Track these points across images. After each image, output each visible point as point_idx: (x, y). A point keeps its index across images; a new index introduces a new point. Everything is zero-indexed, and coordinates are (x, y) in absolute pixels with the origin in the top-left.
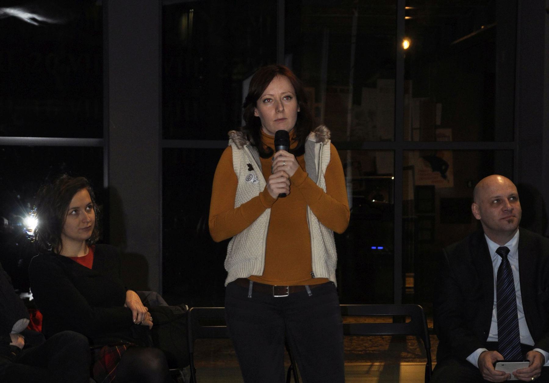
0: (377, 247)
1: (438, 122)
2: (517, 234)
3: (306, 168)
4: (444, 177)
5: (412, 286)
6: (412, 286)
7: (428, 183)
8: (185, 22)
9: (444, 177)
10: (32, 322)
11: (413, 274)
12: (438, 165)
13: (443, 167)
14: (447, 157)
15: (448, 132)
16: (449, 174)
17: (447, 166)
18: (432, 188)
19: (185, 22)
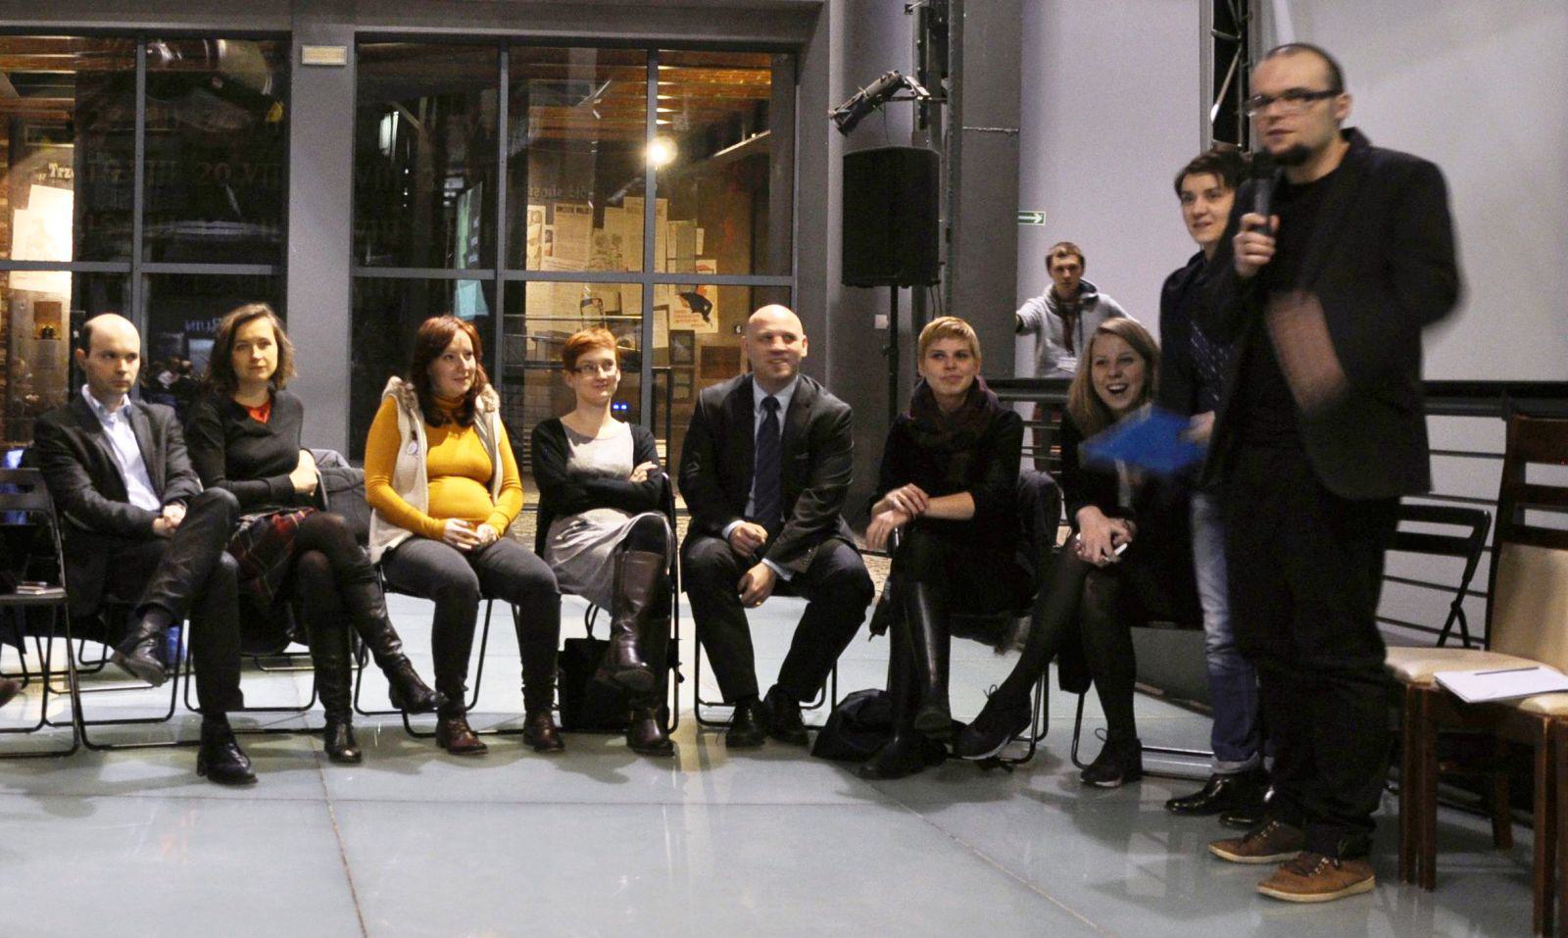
0: (620, 406)
1: (700, 252)
2: (370, 653)
3: (1067, 817)
4: (706, 319)
5: (1396, 561)
6: (1396, 561)
7: (686, 327)
8: (388, 128)
9: (706, 319)
10: (236, 484)
11: (664, 441)
12: (698, 304)
13: (706, 308)
14: (711, 293)
15: (712, 264)
16: (713, 315)
17: (710, 306)
18: (691, 334)
19: (388, 128)
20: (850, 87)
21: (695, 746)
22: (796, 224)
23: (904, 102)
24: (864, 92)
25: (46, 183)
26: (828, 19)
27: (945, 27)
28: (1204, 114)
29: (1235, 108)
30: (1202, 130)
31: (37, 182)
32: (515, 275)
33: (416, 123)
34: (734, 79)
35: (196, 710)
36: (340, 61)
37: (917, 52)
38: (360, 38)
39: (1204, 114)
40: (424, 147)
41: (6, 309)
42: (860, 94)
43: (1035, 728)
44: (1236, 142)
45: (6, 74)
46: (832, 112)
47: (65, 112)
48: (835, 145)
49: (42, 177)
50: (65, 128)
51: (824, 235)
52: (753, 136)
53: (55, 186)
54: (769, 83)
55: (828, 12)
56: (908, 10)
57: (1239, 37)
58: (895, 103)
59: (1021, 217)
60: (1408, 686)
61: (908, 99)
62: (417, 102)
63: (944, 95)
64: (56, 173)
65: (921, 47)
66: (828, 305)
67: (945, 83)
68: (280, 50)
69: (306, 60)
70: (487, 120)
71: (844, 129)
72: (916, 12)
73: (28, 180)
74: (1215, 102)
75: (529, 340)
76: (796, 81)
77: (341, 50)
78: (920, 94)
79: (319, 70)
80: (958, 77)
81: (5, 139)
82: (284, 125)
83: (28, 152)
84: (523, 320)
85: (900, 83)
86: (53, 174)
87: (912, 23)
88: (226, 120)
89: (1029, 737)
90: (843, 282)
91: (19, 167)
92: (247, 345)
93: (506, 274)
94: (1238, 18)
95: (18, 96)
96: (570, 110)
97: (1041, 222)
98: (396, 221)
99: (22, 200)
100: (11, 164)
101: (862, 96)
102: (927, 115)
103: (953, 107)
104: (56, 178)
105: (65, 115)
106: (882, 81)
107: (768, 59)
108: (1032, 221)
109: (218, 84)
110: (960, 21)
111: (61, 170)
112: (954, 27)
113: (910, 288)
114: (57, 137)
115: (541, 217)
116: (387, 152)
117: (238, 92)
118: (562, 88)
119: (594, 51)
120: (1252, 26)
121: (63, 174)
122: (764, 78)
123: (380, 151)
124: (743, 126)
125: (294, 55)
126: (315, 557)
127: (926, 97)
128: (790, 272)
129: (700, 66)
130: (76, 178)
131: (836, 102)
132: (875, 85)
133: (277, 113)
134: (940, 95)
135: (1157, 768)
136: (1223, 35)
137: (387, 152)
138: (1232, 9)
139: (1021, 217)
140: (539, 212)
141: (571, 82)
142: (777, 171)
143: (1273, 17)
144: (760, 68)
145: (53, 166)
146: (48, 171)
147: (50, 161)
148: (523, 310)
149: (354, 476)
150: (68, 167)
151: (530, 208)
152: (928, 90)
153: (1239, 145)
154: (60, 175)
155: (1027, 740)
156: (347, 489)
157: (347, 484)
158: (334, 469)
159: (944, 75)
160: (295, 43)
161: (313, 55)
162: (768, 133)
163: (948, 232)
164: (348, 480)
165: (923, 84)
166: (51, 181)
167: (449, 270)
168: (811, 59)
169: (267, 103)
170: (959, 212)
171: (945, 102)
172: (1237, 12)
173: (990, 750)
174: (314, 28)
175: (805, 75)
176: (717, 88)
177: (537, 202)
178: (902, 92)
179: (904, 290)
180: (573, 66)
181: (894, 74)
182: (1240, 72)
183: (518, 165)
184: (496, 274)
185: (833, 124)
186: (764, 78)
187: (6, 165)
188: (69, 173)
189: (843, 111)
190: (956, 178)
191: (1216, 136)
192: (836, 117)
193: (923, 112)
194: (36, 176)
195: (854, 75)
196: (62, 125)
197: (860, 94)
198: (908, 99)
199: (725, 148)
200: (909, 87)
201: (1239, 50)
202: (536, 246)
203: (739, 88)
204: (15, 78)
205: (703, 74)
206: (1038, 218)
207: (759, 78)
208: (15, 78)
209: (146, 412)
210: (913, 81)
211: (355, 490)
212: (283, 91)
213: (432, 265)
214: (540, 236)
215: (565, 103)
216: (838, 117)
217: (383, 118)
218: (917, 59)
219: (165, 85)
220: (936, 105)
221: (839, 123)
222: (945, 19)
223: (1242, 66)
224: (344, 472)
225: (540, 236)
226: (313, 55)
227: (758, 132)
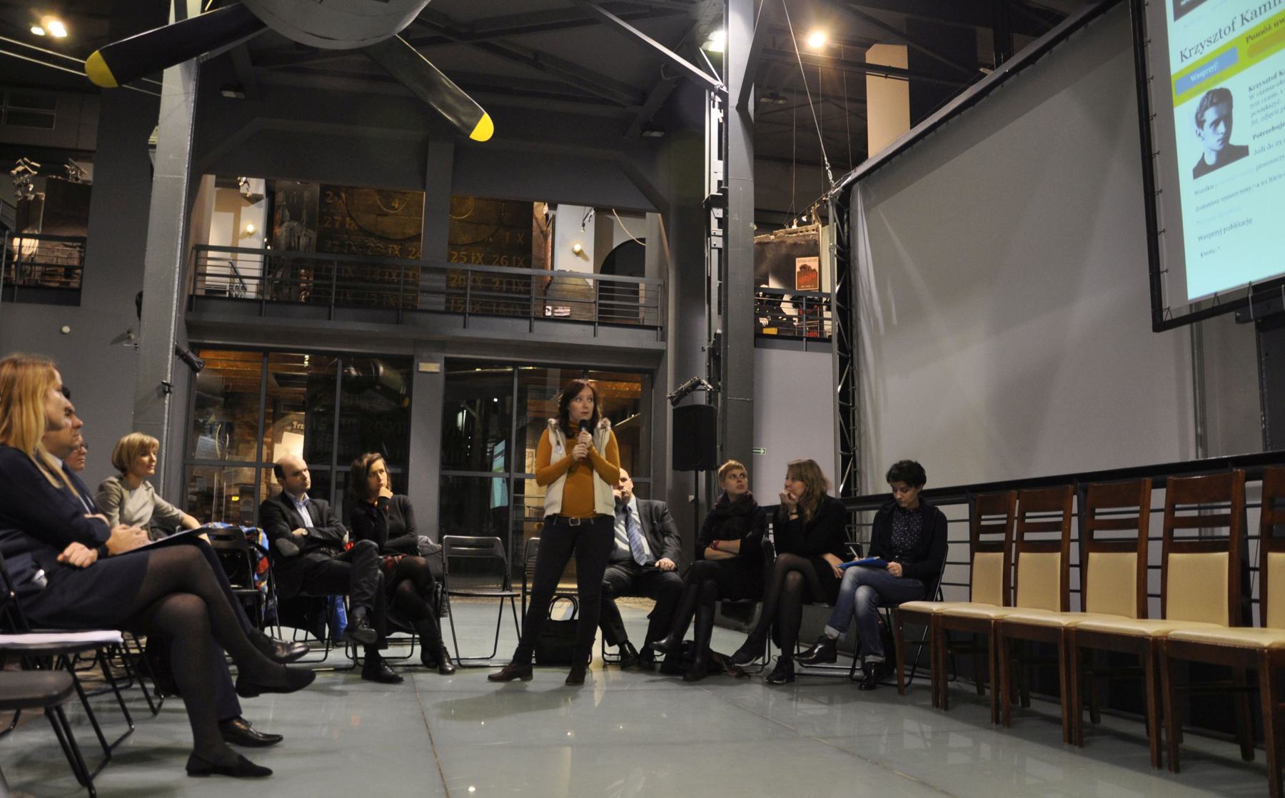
8: (461, 418)
19: (461, 418)
20: (677, 384)
25: (291, 431)
28: (835, 389)
32: (519, 476)
34: (624, 387)
38: (446, 359)
39: (835, 389)
40: (478, 426)
56: (703, 350)
65: (709, 367)
68: (405, 365)
71: (673, 404)
73: (283, 429)
80: (726, 379)
82: (410, 407)
83: (283, 415)
85: (699, 383)
87: (705, 356)
91: (278, 423)
92: (375, 474)
94: (849, 347)
96: (547, 402)
98: (461, 453)
105: (302, 398)
110: (726, 349)
114: (297, 409)
117: (389, 392)
118: (544, 391)
123: (457, 428)
126: (405, 585)
131: (670, 391)
132: (688, 383)
134: (717, 388)
135: (869, 476)
142: (643, 429)
148: (523, 492)
160: (416, 361)
161: (425, 367)
166: (296, 431)
174: (425, 354)
178: (700, 387)
186: (637, 387)
188: (302, 426)
190: (724, 420)
204: (277, 377)
205: (609, 384)
208: (277, 377)
209: (314, 504)
210: (704, 382)
213: (481, 470)
216: (671, 398)
220: (716, 393)
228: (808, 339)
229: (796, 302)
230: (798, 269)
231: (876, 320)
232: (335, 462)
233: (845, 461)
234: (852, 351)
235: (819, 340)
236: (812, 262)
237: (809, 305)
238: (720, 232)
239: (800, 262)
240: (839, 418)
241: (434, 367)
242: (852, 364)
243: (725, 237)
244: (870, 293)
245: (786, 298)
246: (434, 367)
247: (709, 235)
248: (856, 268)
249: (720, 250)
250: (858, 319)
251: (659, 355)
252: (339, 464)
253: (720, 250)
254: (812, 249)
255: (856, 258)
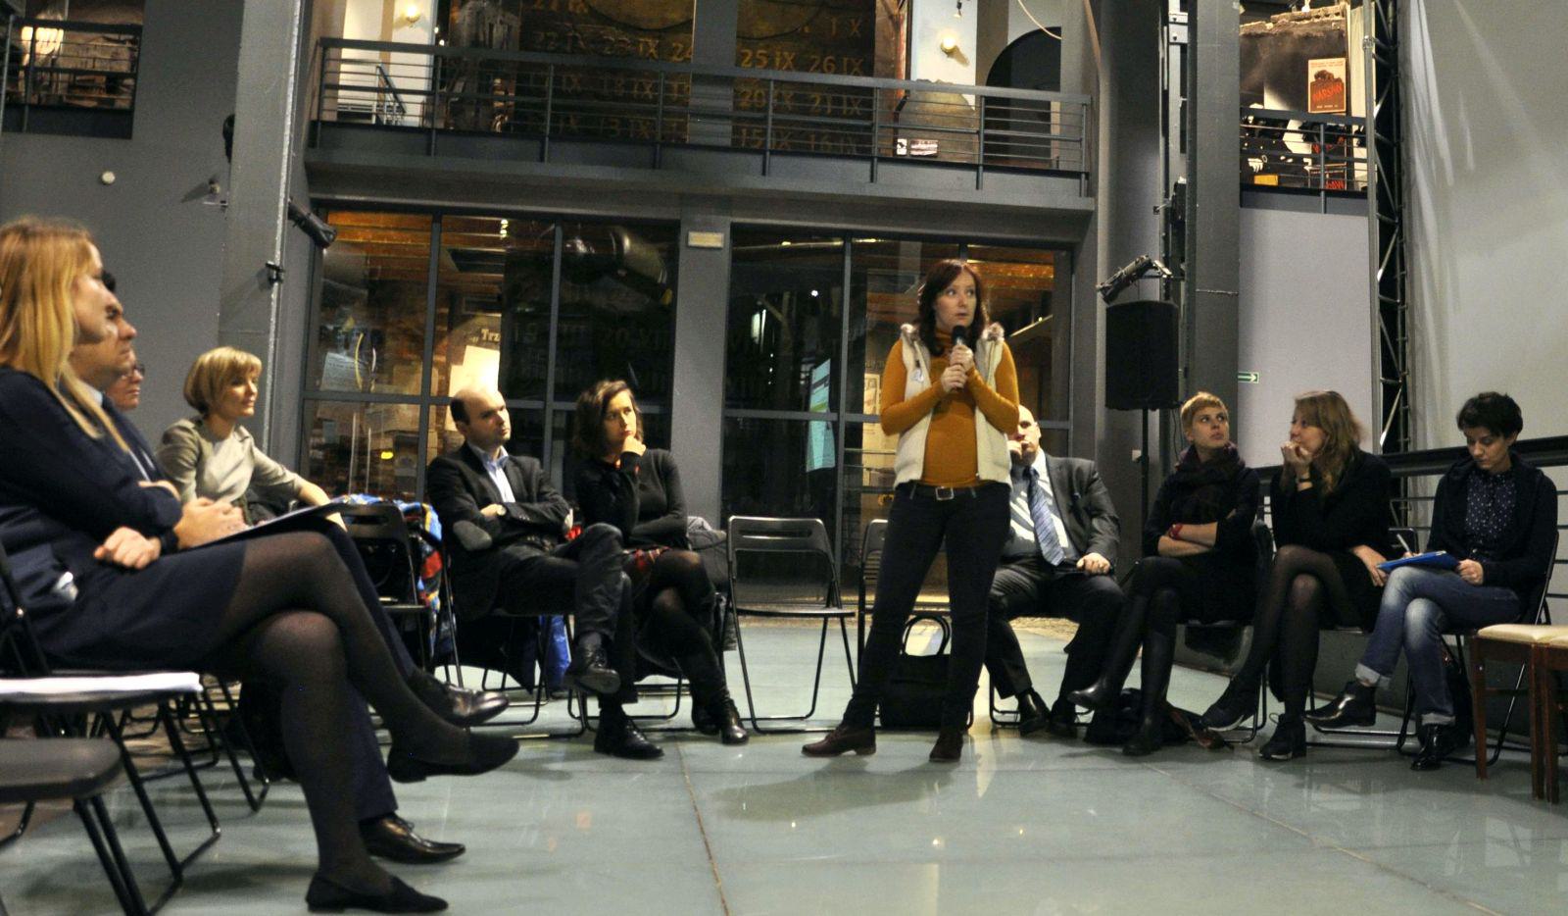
8: (758, 323)
19: (758, 323)
20: (1113, 266)
21: (991, 741)
22: (1072, 381)
23: (1153, 280)
24: (1122, 271)
25: (479, 344)
26: (1096, 224)
27: (1182, 222)
28: (1372, 275)
29: (1398, 437)
30: (1371, 286)
31: (471, 344)
32: (854, 418)
33: (779, 316)
34: (1026, 272)
35: (578, 718)
36: (719, 245)
37: (1162, 241)
39: (1372, 275)
40: (786, 337)
41: (441, 446)
42: (1119, 273)
43: (1256, 721)
44: (1398, 379)
45: (449, 251)
46: (1099, 286)
47: (496, 286)
48: (1101, 307)
49: (475, 339)
50: (495, 300)
51: (1093, 389)
52: (1040, 319)
53: (486, 347)
54: (1052, 276)
55: (1096, 218)
57: (1398, 301)
58: (1147, 280)
59: (1240, 377)
60: (1533, 646)
61: (1157, 277)
62: (781, 297)
63: (1182, 274)
64: (487, 337)
65: (1166, 239)
66: (1096, 444)
67: (1183, 267)
69: (692, 243)
70: (835, 312)
71: (1107, 299)
72: (1162, 212)
73: (465, 342)
74: (1380, 268)
75: (865, 470)
76: (1072, 272)
77: (720, 236)
78: (1164, 273)
79: (698, 251)
80: (1193, 260)
81: (446, 307)
83: (465, 319)
84: (860, 455)
85: (1149, 265)
86: (484, 338)
87: (1158, 221)
88: (627, 301)
89: (1251, 727)
90: (1106, 405)
93: (847, 417)
94: (1395, 206)
95: (457, 270)
96: (899, 296)
97: (1256, 380)
99: (459, 359)
100: (450, 329)
101: (1122, 274)
102: (1170, 286)
103: (1188, 283)
104: (487, 340)
105: (497, 290)
106: (1137, 263)
107: (1049, 255)
108: (1249, 380)
109: (622, 273)
110: (1194, 210)
111: (492, 335)
112: (1190, 215)
113: (1158, 411)
114: (488, 308)
115: (876, 382)
116: (757, 341)
118: (894, 279)
119: (919, 244)
120: (1405, 212)
121: (493, 337)
122: (1047, 272)
123: (752, 340)
124: (1033, 311)
125: (682, 237)
127: (1169, 276)
128: (1068, 418)
129: (1000, 261)
130: (502, 339)
131: (1102, 279)
132: (1131, 265)
133: (668, 299)
134: (1179, 274)
136: (1385, 218)
137: (757, 341)
138: (1392, 353)
139: (1240, 377)
140: (875, 379)
141: (901, 272)
143: (1419, 204)
144: (1046, 264)
145: (485, 331)
146: (481, 335)
147: (483, 327)
149: (716, 537)
150: (496, 332)
151: (867, 375)
152: (1171, 270)
153: (1398, 301)
154: (490, 339)
155: (1249, 729)
156: (710, 546)
157: (710, 543)
158: (701, 531)
159: (1183, 260)
161: (697, 239)
162: (1051, 316)
163: (1186, 370)
164: (711, 539)
165: (1167, 265)
167: (805, 413)
168: (1083, 256)
169: (662, 289)
170: (1193, 345)
171: (1183, 279)
172: (1394, 200)
173: (1218, 727)
174: (698, 218)
175: (1078, 269)
176: (1012, 280)
177: (873, 371)
178: (1151, 272)
179: (1153, 413)
180: (902, 259)
181: (1145, 257)
182: (1398, 246)
183: (858, 346)
184: (839, 417)
185: (1099, 295)
187: (446, 329)
188: (497, 337)
189: (1107, 285)
190: (1191, 326)
191: (1381, 292)
192: (1101, 290)
193: (1167, 287)
194: (471, 339)
195: (1115, 262)
196: (494, 298)
197: (1119, 273)
198: (1157, 277)
199: (1019, 329)
200: (1156, 268)
201: (1397, 230)
202: (872, 406)
203: (1028, 280)
204: (456, 255)
206: (1253, 378)
207: (1044, 272)
208: (456, 255)
210: (1158, 263)
211: (717, 548)
212: (673, 283)
214: (875, 397)
215: (895, 291)
217: (754, 313)
218: (1162, 247)
219: (579, 271)
221: (1104, 294)
222: (1183, 217)
223: (1398, 242)
224: (709, 533)
225: (875, 397)
226: (697, 239)
227: (1043, 316)
228: (1329, 193)
229: (1309, 133)
230: (1311, 79)
231: (1440, 162)
232: (550, 395)
233: (1389, 393)
234: (1400, 214)
235: (1346, 194)
236: (1335, 67)
237: (1332, 137)
238: (1184, 17)
239: (1314, 67)
240: (1379, 323)
241: (714, 240)
242: (1400, 235)
243: (1192, 25)
244: (1430, 117)
245: (1293, 125)
246: (714, 240)
247: (1166, 22)
248: (1408, 77)
249: (1183, 47)
250: (1410, 159)
251: (1085, 219)
252: (556, 398)
253: (1183, 47)
254: (1336, 45)
255: (1407, 60)
